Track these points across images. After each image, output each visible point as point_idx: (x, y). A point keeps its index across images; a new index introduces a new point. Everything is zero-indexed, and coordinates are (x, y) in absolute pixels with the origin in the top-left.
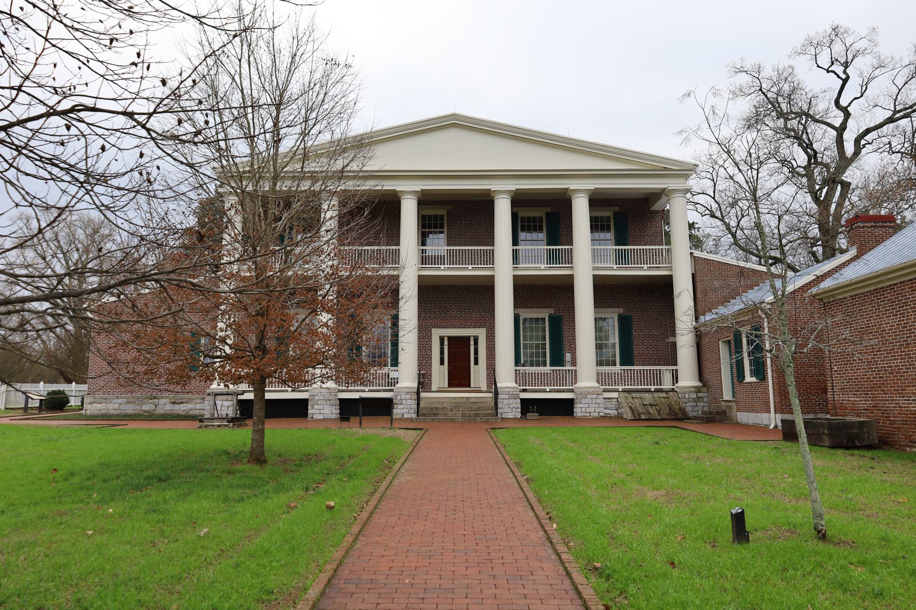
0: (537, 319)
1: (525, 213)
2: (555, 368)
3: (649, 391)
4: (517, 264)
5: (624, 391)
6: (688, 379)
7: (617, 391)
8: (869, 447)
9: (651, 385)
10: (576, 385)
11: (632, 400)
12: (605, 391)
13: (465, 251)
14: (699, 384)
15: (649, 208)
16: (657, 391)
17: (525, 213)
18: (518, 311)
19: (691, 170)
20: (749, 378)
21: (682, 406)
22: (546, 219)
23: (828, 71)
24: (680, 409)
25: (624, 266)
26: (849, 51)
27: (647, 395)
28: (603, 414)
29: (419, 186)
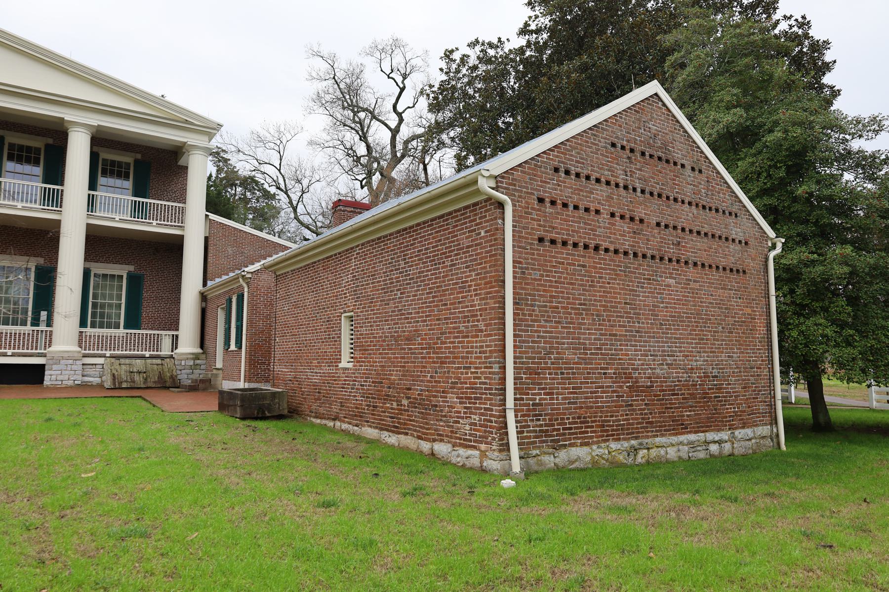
0: (113, 276)
1: (106, 155)
2: (129, 331)
3: (143, 357)
4: (92, 212)
5: (112, 357)
6: (188, 345)
7: (104, 356)
8: (280, 417)
9: (106, 350)
10: (50, 349)
11: (118, 367)
12: (85, 356)
13: (158, 206)
14: (200, 351)
15: (177, 162)
16: (151, 357)
17: (106, 155)
18: (88, 265)
19: (214, 129)
20: (233, 347)
21: (175, 374)
22: (135, 166)
23: (389, 77)
24: (172, 377)
25: (140, 220)
26: (408, 65)
27: (138, 361)
28: (79, 382)
29: (96, 120)
